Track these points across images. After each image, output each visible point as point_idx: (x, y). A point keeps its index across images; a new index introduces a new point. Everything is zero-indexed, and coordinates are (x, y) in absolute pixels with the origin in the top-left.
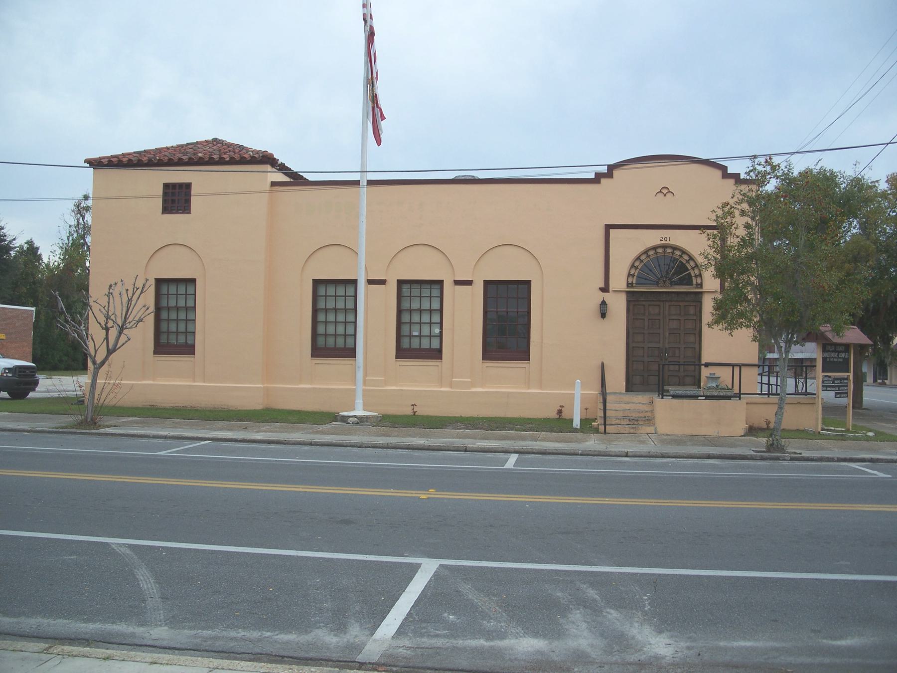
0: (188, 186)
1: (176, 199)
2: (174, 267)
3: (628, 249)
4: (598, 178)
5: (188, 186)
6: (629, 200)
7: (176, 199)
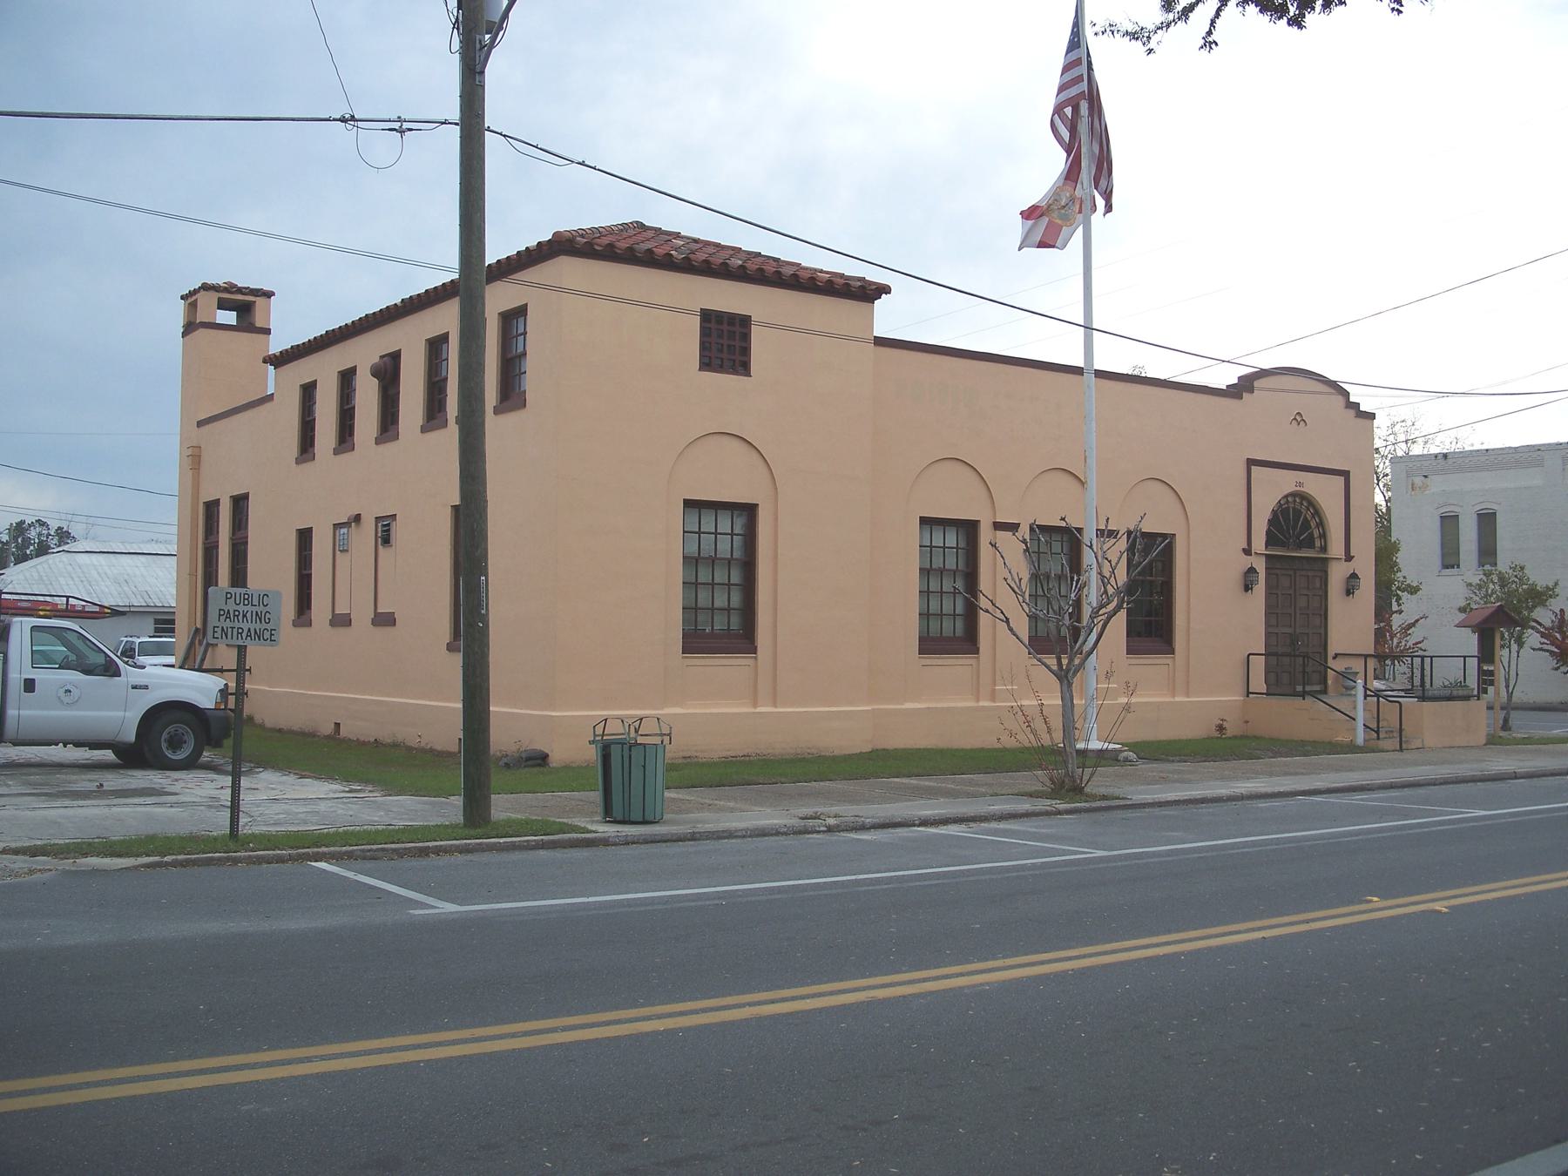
1: (725, 344)
3: (1272, 490)
7: (725, 344)
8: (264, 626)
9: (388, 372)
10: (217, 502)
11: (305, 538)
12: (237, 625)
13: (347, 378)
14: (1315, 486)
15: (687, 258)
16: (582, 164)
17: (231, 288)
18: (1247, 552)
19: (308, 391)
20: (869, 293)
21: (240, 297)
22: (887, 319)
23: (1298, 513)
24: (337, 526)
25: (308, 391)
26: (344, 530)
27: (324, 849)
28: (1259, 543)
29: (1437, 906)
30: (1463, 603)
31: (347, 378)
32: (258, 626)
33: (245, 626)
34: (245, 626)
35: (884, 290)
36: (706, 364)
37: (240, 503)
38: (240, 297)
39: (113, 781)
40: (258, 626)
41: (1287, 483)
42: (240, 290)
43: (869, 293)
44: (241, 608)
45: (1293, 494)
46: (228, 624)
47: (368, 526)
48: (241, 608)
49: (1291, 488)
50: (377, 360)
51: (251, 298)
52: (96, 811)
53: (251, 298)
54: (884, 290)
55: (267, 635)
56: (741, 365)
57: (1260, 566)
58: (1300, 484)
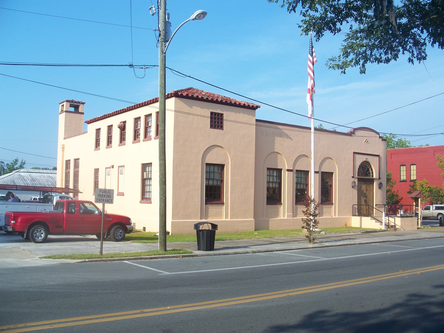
0: (222, 115)
1: (217, 121)
2: (214, 158)
3: (360, 159)
4: (350, 134)
5: (222, 115)
6: (358, 143)
7: (217, 121)
8: (109, 198)
9: (123, 128)
10: (70, 160)
11: (97, 171)
12: (102, 198)
13: (110, 128)
14: (370, 159)
15: (207, 98)
16: (190, 77)
17: (72, 101)
18: (353, 177)
19: (98, 131)
20: (254, 108)
21: (76, 104)
22: (260, 114)
23: (366, 166)
24: (106, 168)
25: (98, 131)
26: (109, 169)
27: (93, 259)
28: (356, 176)
29: (417, 272)
30: (408, 191)
31: (110, 128)
32: (108, 199)
33: (105, 199)
34: (105, 199)
35: (258, 107)
36: (211, 127)
37: (76, 161)
38: (76, 104)
39: (363, 236)
40: (108, 199)
41: (364, 158)
42: (76, 102)
43: (254, 108)
44: (104, 194)
45: (365, 161)
46: (100, 198)
47: (116, 167)
48: (104, 194)
49: (365, 160)
50: (119, 123)
51: (78, 104)
52: (45, 247)
53: (78, 104)
54: (258, 107)
55: (110, 201)
56: (221, 127)
57: (356, 181)
58: (367, 159)
